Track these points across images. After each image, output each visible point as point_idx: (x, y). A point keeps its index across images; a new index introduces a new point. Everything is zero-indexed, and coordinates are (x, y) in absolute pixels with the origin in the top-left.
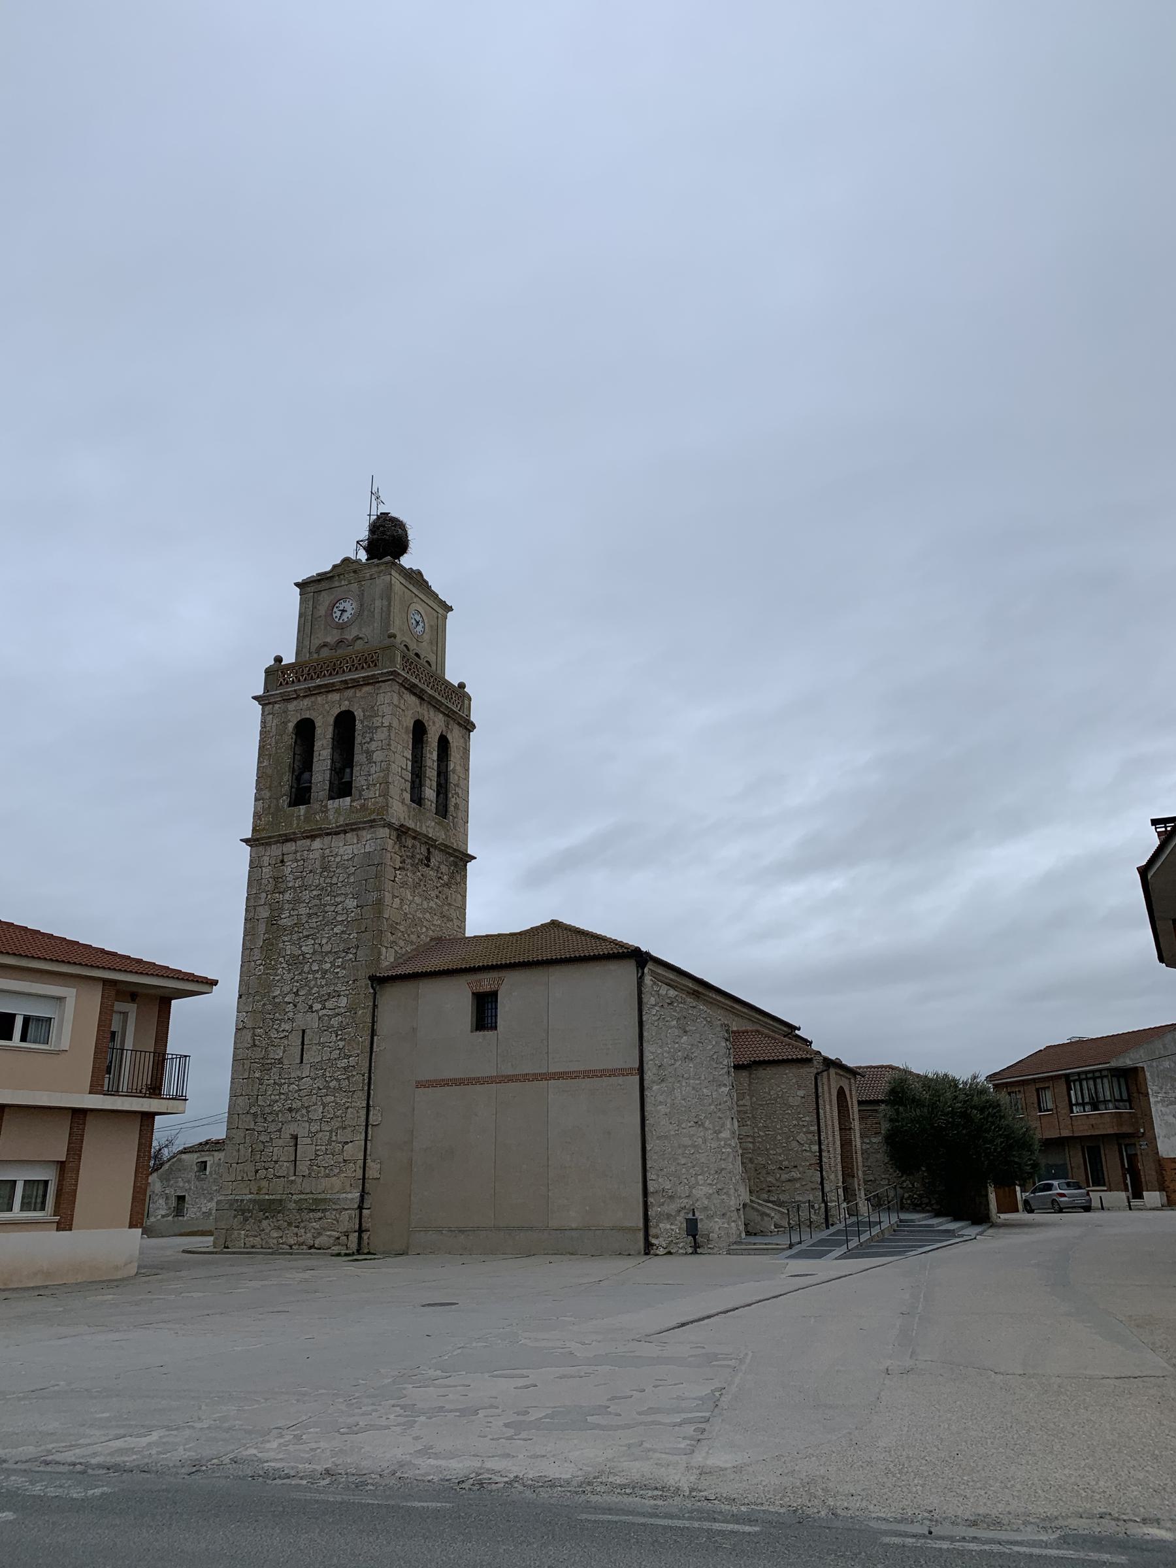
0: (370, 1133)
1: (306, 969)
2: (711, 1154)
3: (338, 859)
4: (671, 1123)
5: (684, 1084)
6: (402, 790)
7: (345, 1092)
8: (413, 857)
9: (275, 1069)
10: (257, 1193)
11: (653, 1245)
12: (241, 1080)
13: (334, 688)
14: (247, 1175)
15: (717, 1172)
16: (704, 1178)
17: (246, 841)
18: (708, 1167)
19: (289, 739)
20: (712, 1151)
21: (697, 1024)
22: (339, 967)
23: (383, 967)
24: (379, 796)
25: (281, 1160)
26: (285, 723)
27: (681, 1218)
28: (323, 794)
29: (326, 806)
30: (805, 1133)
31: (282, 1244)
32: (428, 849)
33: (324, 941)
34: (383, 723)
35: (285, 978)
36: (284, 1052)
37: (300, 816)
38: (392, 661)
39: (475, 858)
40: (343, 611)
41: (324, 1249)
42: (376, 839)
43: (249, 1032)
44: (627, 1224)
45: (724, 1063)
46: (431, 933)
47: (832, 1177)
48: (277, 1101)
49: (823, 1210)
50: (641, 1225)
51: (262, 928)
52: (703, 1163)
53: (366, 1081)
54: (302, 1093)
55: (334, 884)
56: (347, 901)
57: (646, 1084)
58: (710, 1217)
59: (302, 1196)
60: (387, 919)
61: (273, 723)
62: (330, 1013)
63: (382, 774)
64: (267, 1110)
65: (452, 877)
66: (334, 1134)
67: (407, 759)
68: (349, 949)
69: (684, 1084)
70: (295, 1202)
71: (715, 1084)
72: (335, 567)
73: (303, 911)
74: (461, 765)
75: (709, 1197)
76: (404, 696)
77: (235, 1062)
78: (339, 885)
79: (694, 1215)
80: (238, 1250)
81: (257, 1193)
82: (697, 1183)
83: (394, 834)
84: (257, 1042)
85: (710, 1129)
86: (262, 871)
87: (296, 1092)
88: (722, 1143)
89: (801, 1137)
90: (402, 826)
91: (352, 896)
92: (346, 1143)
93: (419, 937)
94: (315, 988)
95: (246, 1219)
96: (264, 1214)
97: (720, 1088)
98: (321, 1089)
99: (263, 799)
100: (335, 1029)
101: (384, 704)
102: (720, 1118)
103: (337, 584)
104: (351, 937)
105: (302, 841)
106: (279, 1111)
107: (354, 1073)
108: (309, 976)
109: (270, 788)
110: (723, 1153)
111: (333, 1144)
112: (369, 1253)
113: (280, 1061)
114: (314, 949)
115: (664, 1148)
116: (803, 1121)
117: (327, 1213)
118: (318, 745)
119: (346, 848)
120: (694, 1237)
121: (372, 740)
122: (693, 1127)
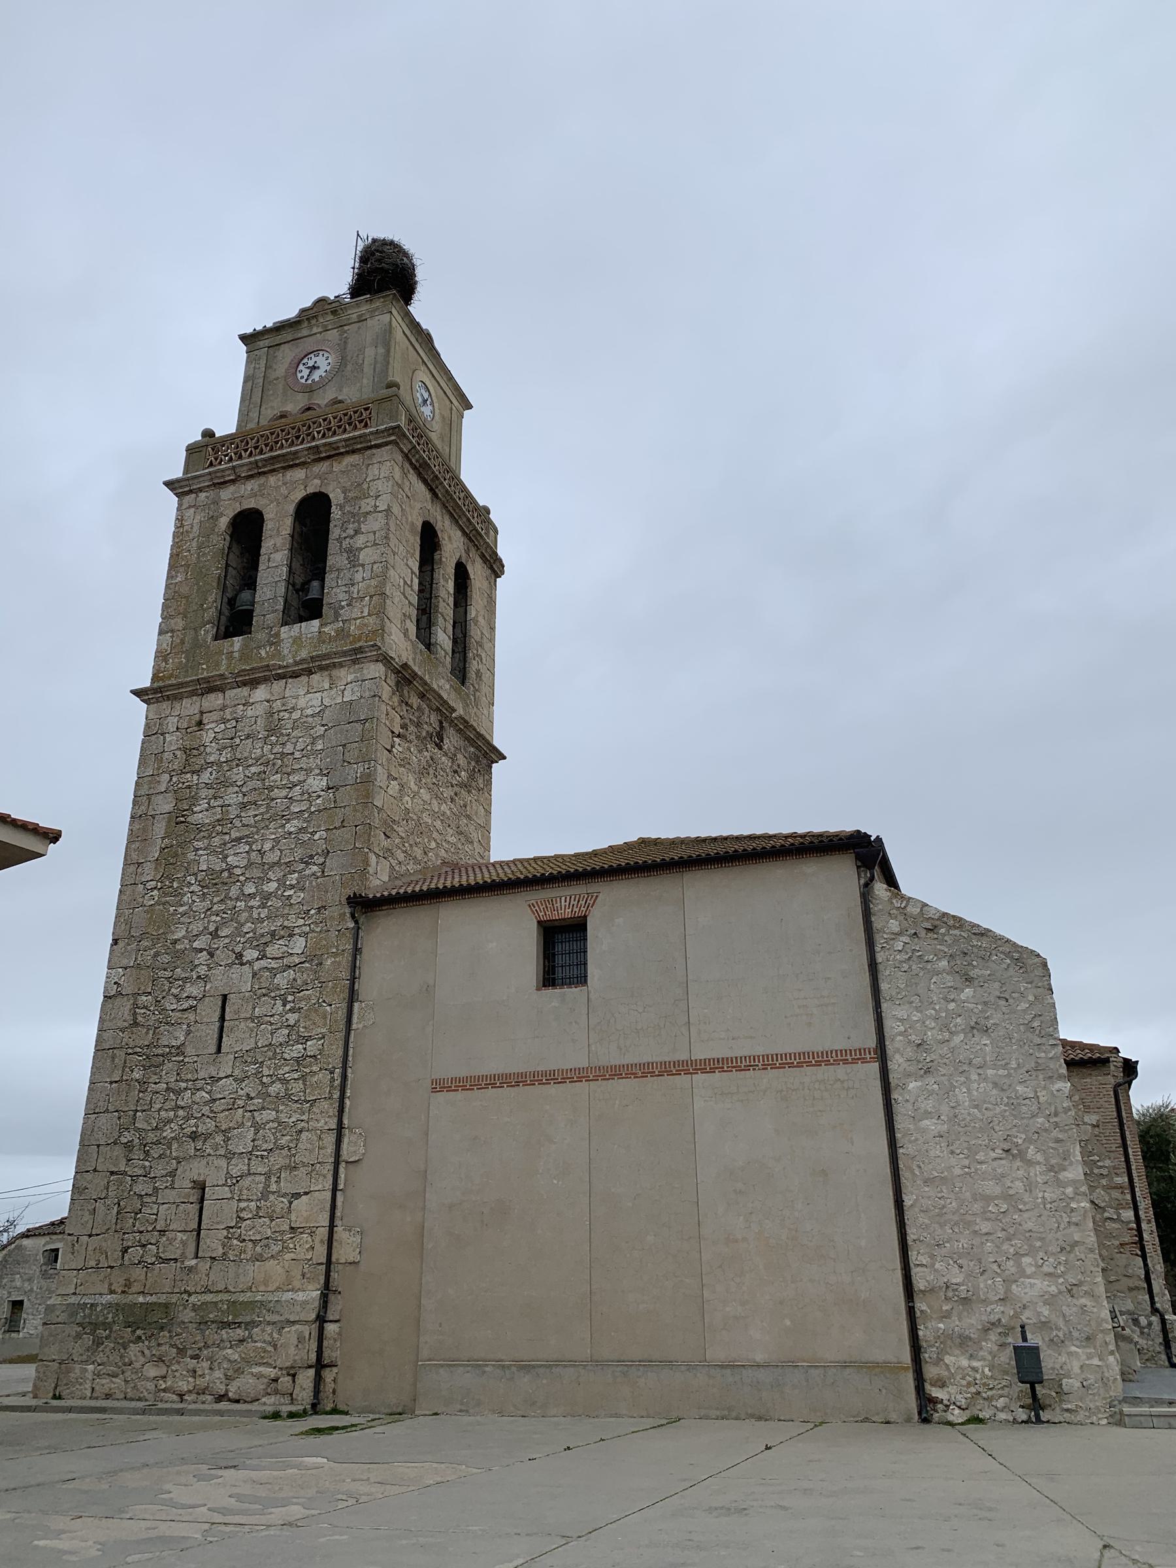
0: (343, 1176)
2: (1046, 1213)
3: (296, 715)
4: (952, 1152)
6: (404, 615)
7: (296, 1101)
8: (418, 725)
9: (170, 1065)
10: (123, 1292)
11: (934, 1401)
12: (106, 1085)
13: (297, 462)
15: (1062, 1249)
17: (138, 693)
18: (1042, 1239)
19: (220, 540)
22: (292, 887)
24: (369, 615)
25: (171, 1228)
26: (214, 519)
28: (273, 618)
29: (277, 635)
31: (164, 1390)
32: (441, 723)
33: (267, 846)
34: (376, 507)
36: (188, 1033)
38: (394, 416)
41: (245, 1402)
44: (879, 1356)
46: (443, 853)
48: (170, 1121)
49: (1157, 1326)
50: (906, 1357)
51: (160, 828)
52: (1030, 1231)
54: (218, 1106)
56: (310, 781)
57: (893, 1078)
59: (209, 1298)
60: (380, 810)
61: (195, 519)
62: (274, 964)
63: (374, 582)
65: (472, 777)
67: (413, 572)
68: (312, 857)
69: (974, 1077)
70: (195, 1308)
71: (1041, 1077)
72: (303, 311)
73: (232, 798)
75: (1050, 1300)
76: (410, 476)
78: (297, 754)
79: (1025, 1339)
80: (80, 1403)
81: (123, 1292)
82: (1022, 1273)
85: (1039, 1163)
87: (206, 1103)
88: (1069, 1190)
90: (405, 666)
91: (318, 771)
92: (297, 1196)
95: (98, 1343)
98: (252, 1098)
101: (379, 479)
102: (1058, 1141)
103: (305, 332)
104: (316, 837)
105: (235, 691)
106: (173, 1138)
107: (315, 1068)
108: (239, 904)
110: (1072, 1210)
111: (272, 1197)
112: (335, 1411)
113: (180, 1050)
116: (1101, 1167)
118: (267, 545)
121: (357, 532)
122: (1001, 1159)
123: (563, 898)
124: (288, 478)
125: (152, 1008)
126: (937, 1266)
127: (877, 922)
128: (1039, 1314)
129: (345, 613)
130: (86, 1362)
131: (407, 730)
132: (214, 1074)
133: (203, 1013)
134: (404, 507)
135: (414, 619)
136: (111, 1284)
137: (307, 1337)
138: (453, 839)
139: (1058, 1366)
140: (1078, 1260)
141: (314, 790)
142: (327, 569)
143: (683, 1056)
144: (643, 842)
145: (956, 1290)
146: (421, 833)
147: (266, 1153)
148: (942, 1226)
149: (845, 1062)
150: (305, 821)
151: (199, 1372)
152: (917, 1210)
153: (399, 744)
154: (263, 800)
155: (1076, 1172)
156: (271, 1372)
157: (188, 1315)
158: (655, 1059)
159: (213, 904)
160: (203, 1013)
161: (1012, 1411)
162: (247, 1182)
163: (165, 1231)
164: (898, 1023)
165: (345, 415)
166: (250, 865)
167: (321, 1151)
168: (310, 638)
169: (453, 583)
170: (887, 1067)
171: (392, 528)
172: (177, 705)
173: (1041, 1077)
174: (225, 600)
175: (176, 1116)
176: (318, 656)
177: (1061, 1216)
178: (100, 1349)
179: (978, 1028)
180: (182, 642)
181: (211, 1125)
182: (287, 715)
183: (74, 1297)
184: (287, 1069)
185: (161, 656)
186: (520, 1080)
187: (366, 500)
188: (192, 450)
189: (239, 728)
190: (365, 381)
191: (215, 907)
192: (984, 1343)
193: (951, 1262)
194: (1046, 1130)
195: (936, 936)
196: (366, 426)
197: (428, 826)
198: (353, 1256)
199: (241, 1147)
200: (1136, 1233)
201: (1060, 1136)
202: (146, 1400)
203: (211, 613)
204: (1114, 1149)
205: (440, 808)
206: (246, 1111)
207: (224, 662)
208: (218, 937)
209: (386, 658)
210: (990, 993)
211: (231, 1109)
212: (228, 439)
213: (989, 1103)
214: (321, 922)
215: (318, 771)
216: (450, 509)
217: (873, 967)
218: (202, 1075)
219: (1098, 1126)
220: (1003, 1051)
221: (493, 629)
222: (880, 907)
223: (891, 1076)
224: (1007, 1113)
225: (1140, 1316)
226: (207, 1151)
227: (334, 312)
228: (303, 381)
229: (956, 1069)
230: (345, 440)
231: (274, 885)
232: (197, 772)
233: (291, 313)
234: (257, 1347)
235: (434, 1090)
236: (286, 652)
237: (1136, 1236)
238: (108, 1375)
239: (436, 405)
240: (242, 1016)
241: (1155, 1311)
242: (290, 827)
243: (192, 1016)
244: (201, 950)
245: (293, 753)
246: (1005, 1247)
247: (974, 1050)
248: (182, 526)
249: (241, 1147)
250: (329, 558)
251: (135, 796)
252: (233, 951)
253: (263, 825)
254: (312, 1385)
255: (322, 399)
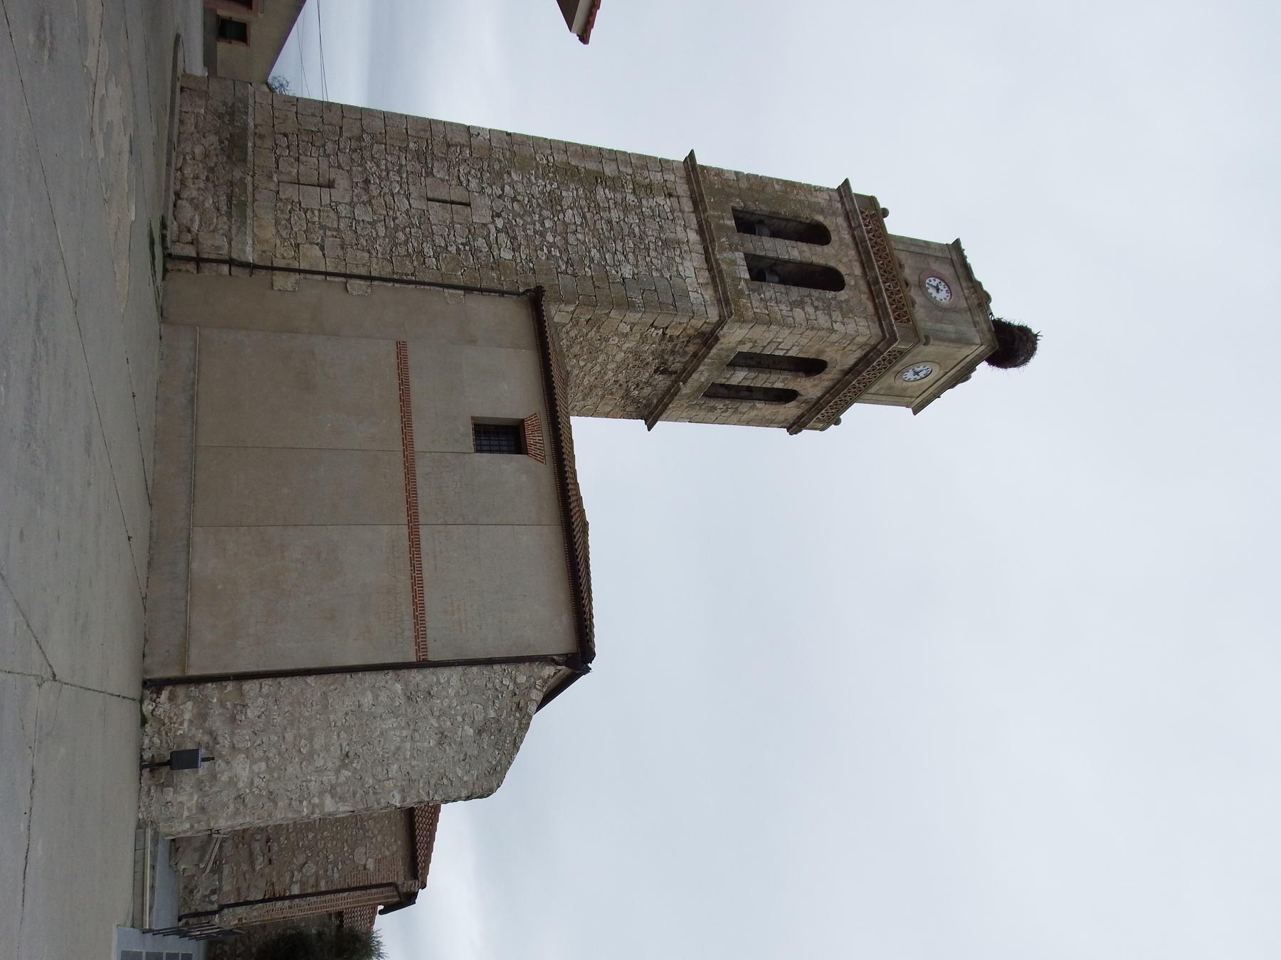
0: (336, 280)
1: (545, 213)
2: (299, 782)
3: (677, 259)
4: (347, 714)
5: (405, 733)
6: (756, 342)
7: (391, 250)
8: (673, 352)
9: (419, 167)
10: (256, 134)
11: (159, 693)
12: (405, 126)
13: (867, 270)
14: (281, 123)
15: (271, 793)
16: (262, 773)
17: (692, 155)
18: (279, 778)
19: (805, 214)
20: (304, 784)
21: (491, 751)
22: (550, 252)
23: (551, 306)
24: (754, 313)
25: (300, 165)
26: (822, 212)
27: (200, 736)
28: (750, 247)
29: (737, 250)
30: (317, 874)
31: (185, 158)
32: (675, 372)
33: (580, 236)
34: (836, 322)
35: (533, 187)
36: (442, 180)
37: (723, 219)
38: (904, 339)
39: (649, 430)
40: (938, 290)
41: (174, 211)
42: (705, 306)
43: (466, 141)
44: (194, 652)
45: (436, 796)
46: (576, 372)
47: (255, 913)
48: (378, 166)
49: (210, 908)
50: (193, 672)
51: (592, 166)
52: (286, 769)
53: (405, 277)
54: (389, 198)
55: (649, 254)
56: (629, 267)
57: (404, 673)
58: (200, 785)
59: (250, 188)
60: (608, 315)
61: (822, 199)
62: (492, 238)
63: (779, 317)
64: (367, 154)
65: (635, 401)
66: (335, 234)
67: (788, 350)
68: (572, 266)
69: (405, 733)
70: (242, 180)
71: (404, 783)
72: (980, 284)
73: (615, 215)
74: (756, 416)
75: (232, 782)
76: (859, 351)
77: (428, 122)
78: (648, 259)
79: (204, 760)
80: (177, 105)
81: (256, 134)
82: (254, 762)
83: (707, 329)
84: (453, 149)
85: (337, 778)
86: (658, 172)
87: (391, 190)
88: (316, 800)
89: (311, 868)
90: (717, 339)
91: (636, 272)
92: (322, 248)
93: (575, 356)
94: (522, 222)
95: (220, 116)
96: (227, 139)
97: (399, 792)
98: (394, 221)
99: (738, 180)
100: (472, 243)
101: (856, 325)
102: (354, 794)
103: (964, 285)
104: (587, 269)
105: (695, 219)
106: (366, 168)
107: (415, 264)
108: (537, 216)
109: (750, 189)
110: (301, 802)
111: (321, 232)
112: (165, 271)
113: (430, 174)
114: (570, 224)
115: (309, 705)
116: (333, 870)
117: (226, 218)
118: (804, 247)
119: (691, 269)
120: (168, 763)
121: (816, 308)
122: (341, 750)
123: (541, 438)
124: (855, 263)
125: (460, 156)
126: (260, 699)
127: (524, 667)
128: (222, 773)
129: (755, 297)
130: (206, 108)
131: (669, 342)
132: (412, 196)
133: (457, 190)
134: (837, 344)
135: (754, 350)
136: (261, 125)
137: (220, 252)
138: (586, 382)
139: (183, 785)
140: (263, 804)
141: (622, 269)
142: (788, 286)
143: (422, 519)
144: (585, 525)
145: (242, 713)
146: (590, 353)
147: (354, 228)
148: (291, 704)
149: (417, 637)
150: (599, 263)
151: (196, 181)
152: (304, 686)
153: (658, 334)
154: (614, 235)
155: (330, 805)
156: (195, 227)
157: (238, 174)
158: (419, 499)
159: (537, 199)
160: (457, 190)
161: (150, 749)
162: (332, 215)
163: (298, 161)
164: (446, 678)
165: (903, 305)
166: (566, 225)
167: (354, 266)
168: (735, 271)
169: (781, 387)
170: (413, 668)
171: (820, 333)
172: (683, 181)
173: (404, 783)
174: (763, 218)
175: (381, 170)
176: (722, 275)
177: (296, 794)
178: (215, 117)
179: (442, 737)
180: (730, 187)
181: (375, 193)
182: (678, 253)
183: (253, 102)
184: (415, 244)
185: (719, 172)
186: (405, 403)
187: (840, 315)
188: (872, 201)
189: (667, 221)
190: (930, 324)
191: (534, 201)
192: (201, 731)
193: (263, 710)
194: (363, 785)
195: (514, 709)
196: (896, 319)
197: (596, 358)
198: (277, 285)
199: (358, 212)
200: (282, 895)
201: (358, 795)
202: (178, 146)
203: (752, 206)
204: (347, 880)
205: (609, 370)
206: (385, 217)
207: (716, 213)
208: (513, 202)
209: (722, 323)
210: (469, 747)
211: (386, 207)
212: (883, 227)
213: (385, 743)
214: (523, 270)
215: (636, 272)
216: (837, 387)
217: (490, 662)
218: (412, 188)
219: (364, 869)
220: (424, 755)
221: (748, 423)
222: (536, 670)
223: (406, 671)
224: (376, 756)
225: (218, 896)
226: (356, 190)
227: (980, 305)
228: (927, 281)
229: (410, 720)
230: (885, 302)
231: (551, 240)
232: (634, 191)
233: (978, 275)
234: (213, 219)
235: (398, 343)
236: (725, 255)
237: (280, 895)
238: (197, 123)
239: (915, 383)
240: (455, 216)
241: (222, 908)
242: (594, 252)
243: (454, 183)
244: (503, 190)
245: (649, 256)
246: (274, 750)
247: (425, 733)
248: (816, 190)
249: (358, 212)
250: (796, 288)
251: (616, 151)
252: (503, 211)
253: (596, 234)
254: (185, 254)
255: (914, 293)
